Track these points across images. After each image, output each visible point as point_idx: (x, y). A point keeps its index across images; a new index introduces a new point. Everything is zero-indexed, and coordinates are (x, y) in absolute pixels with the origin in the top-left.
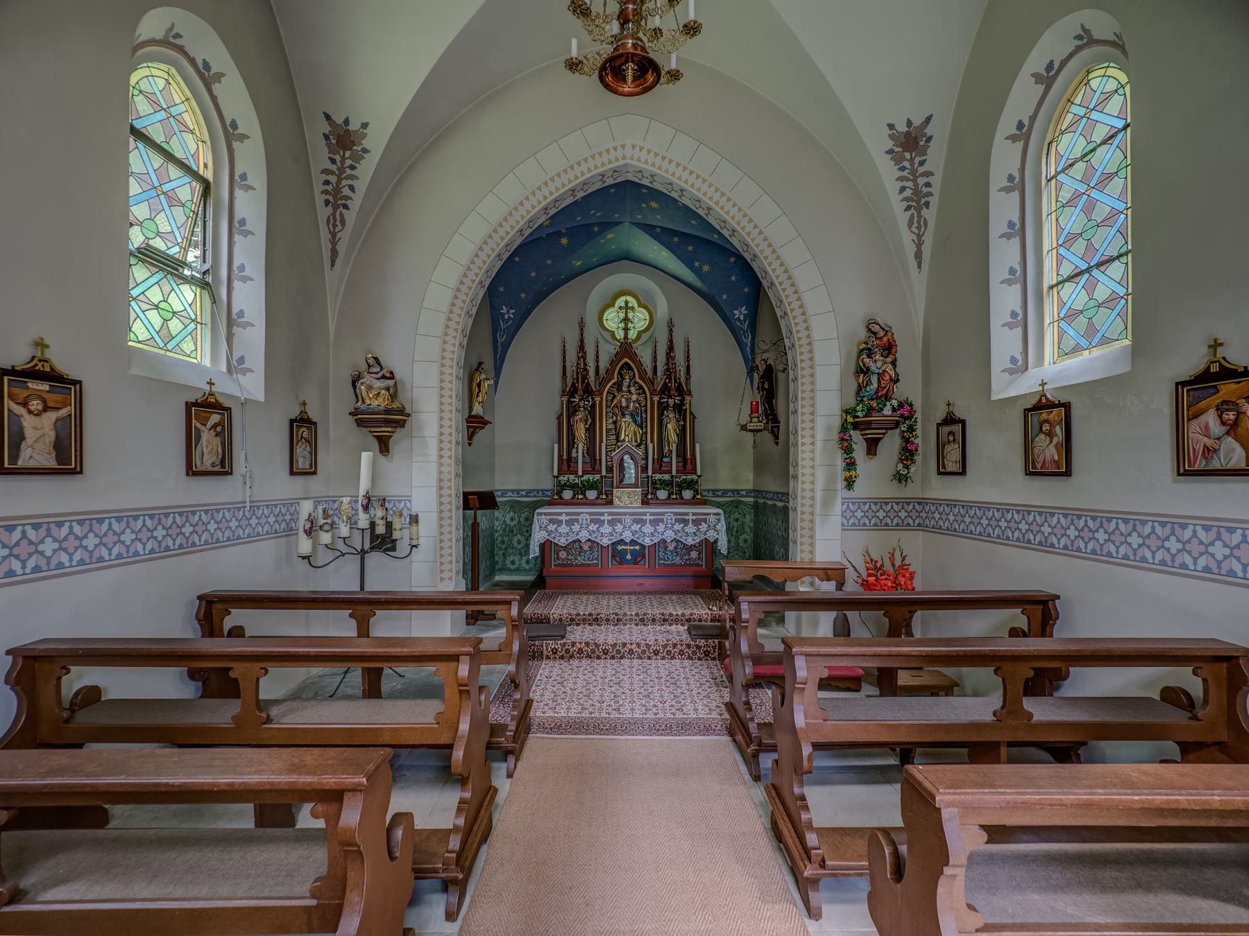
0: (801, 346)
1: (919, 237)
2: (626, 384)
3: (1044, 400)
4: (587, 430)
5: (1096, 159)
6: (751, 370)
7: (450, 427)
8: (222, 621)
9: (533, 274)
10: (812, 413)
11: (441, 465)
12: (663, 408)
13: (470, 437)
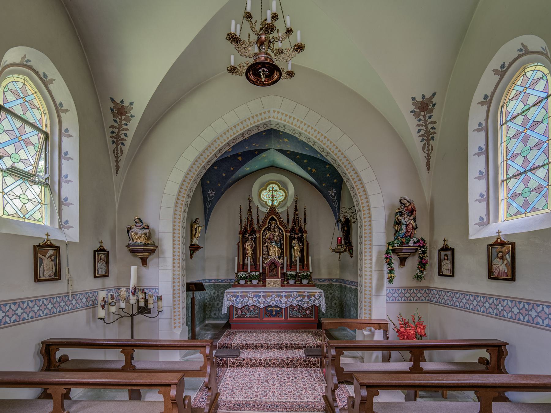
0: (364, 211)
1: (429, 155)
2: (272, 227)
3: (499, 241)
4: (253, 250)
5: (530, 114)
6: (338, 221)
7: (179, 252)
8: (55, 353)
9: (224, 175)
11: (174, 271)
12: (292, 239)
13: (191, 255)
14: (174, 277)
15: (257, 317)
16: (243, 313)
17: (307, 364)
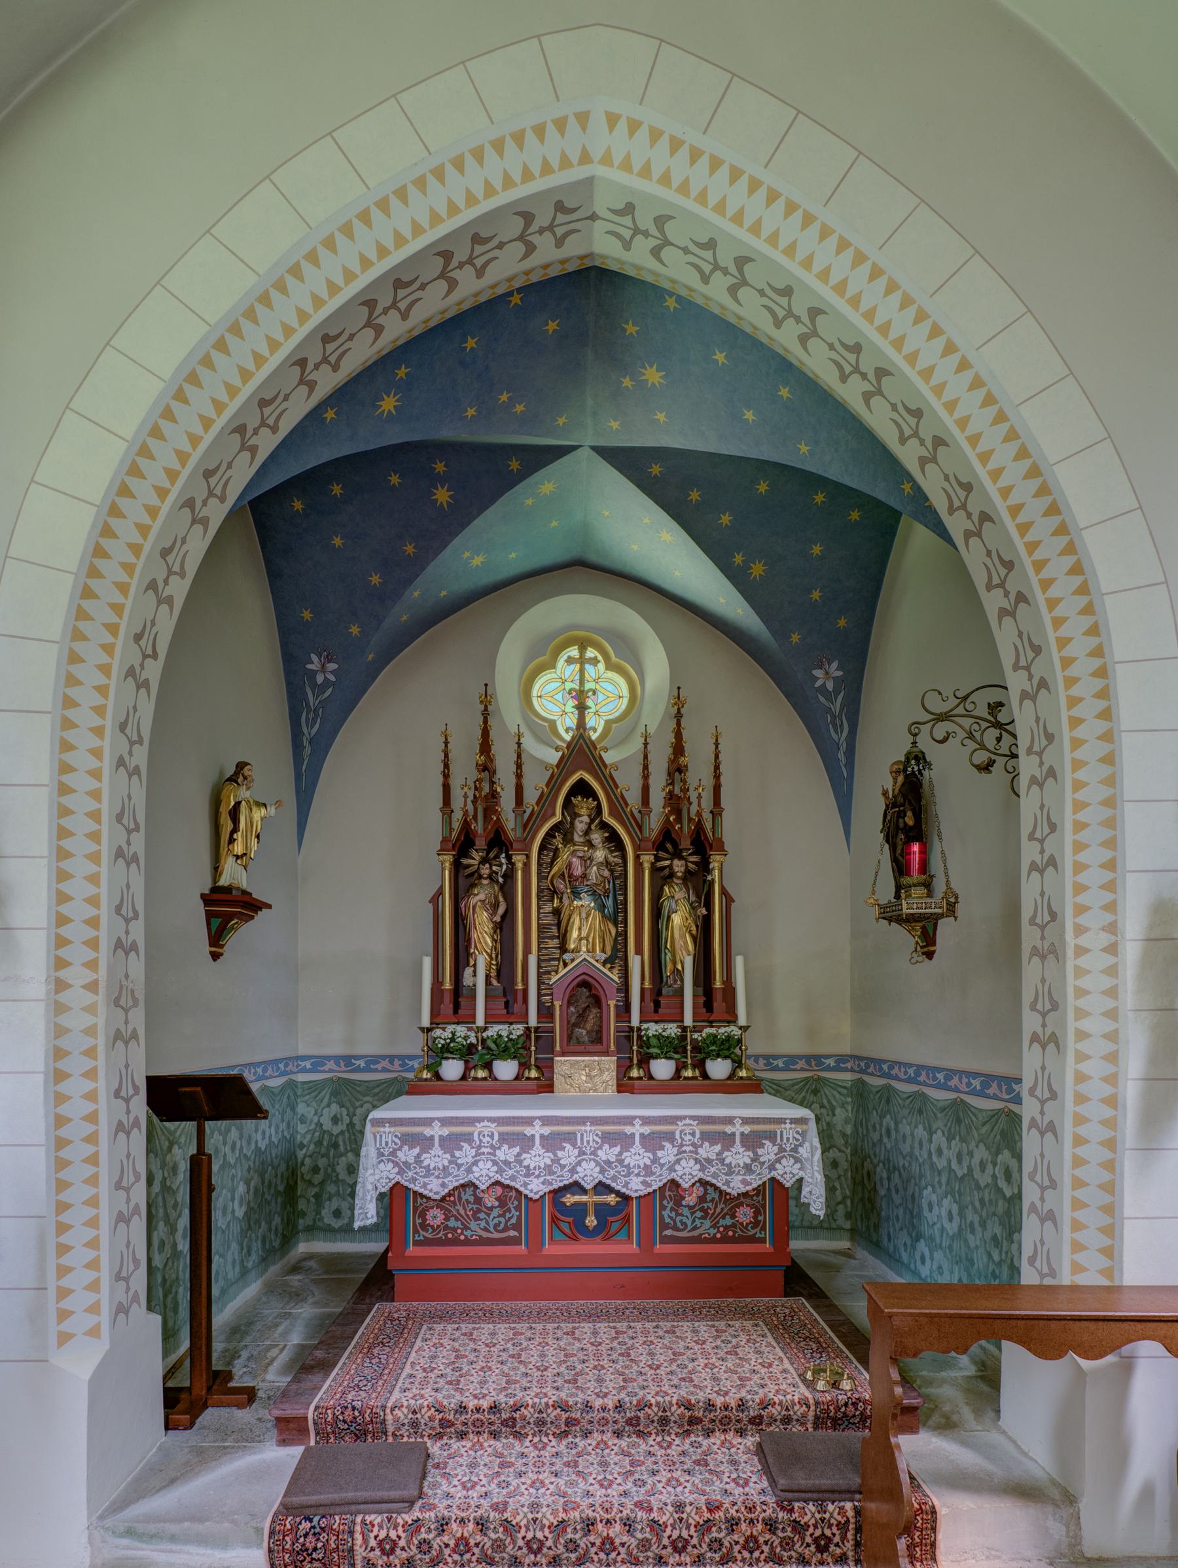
2: (580, 825)
10: (1111, 865)
11: (59, 1008)
12: (662, 877)
14: (63, 1043)
15: (516, 1241)
16: (452, 1223)
17: (787, 1544)
